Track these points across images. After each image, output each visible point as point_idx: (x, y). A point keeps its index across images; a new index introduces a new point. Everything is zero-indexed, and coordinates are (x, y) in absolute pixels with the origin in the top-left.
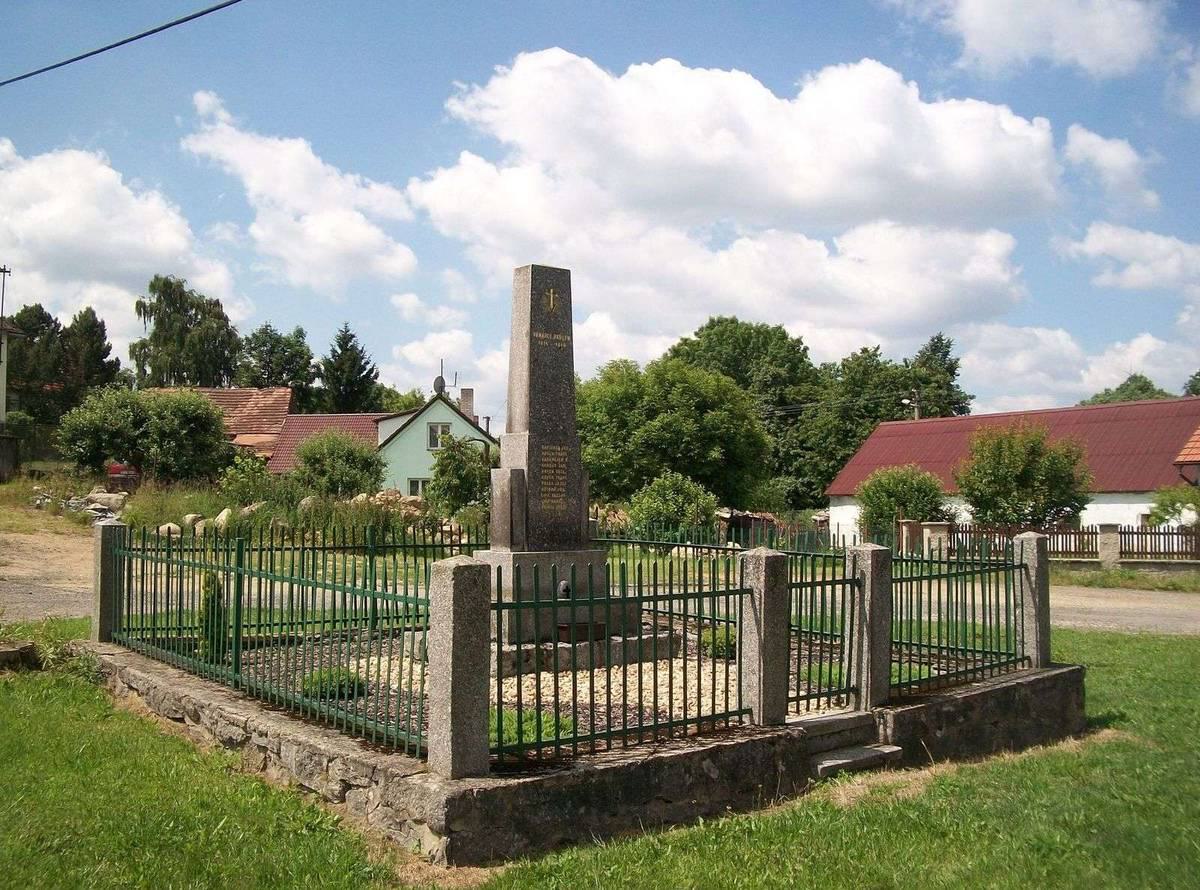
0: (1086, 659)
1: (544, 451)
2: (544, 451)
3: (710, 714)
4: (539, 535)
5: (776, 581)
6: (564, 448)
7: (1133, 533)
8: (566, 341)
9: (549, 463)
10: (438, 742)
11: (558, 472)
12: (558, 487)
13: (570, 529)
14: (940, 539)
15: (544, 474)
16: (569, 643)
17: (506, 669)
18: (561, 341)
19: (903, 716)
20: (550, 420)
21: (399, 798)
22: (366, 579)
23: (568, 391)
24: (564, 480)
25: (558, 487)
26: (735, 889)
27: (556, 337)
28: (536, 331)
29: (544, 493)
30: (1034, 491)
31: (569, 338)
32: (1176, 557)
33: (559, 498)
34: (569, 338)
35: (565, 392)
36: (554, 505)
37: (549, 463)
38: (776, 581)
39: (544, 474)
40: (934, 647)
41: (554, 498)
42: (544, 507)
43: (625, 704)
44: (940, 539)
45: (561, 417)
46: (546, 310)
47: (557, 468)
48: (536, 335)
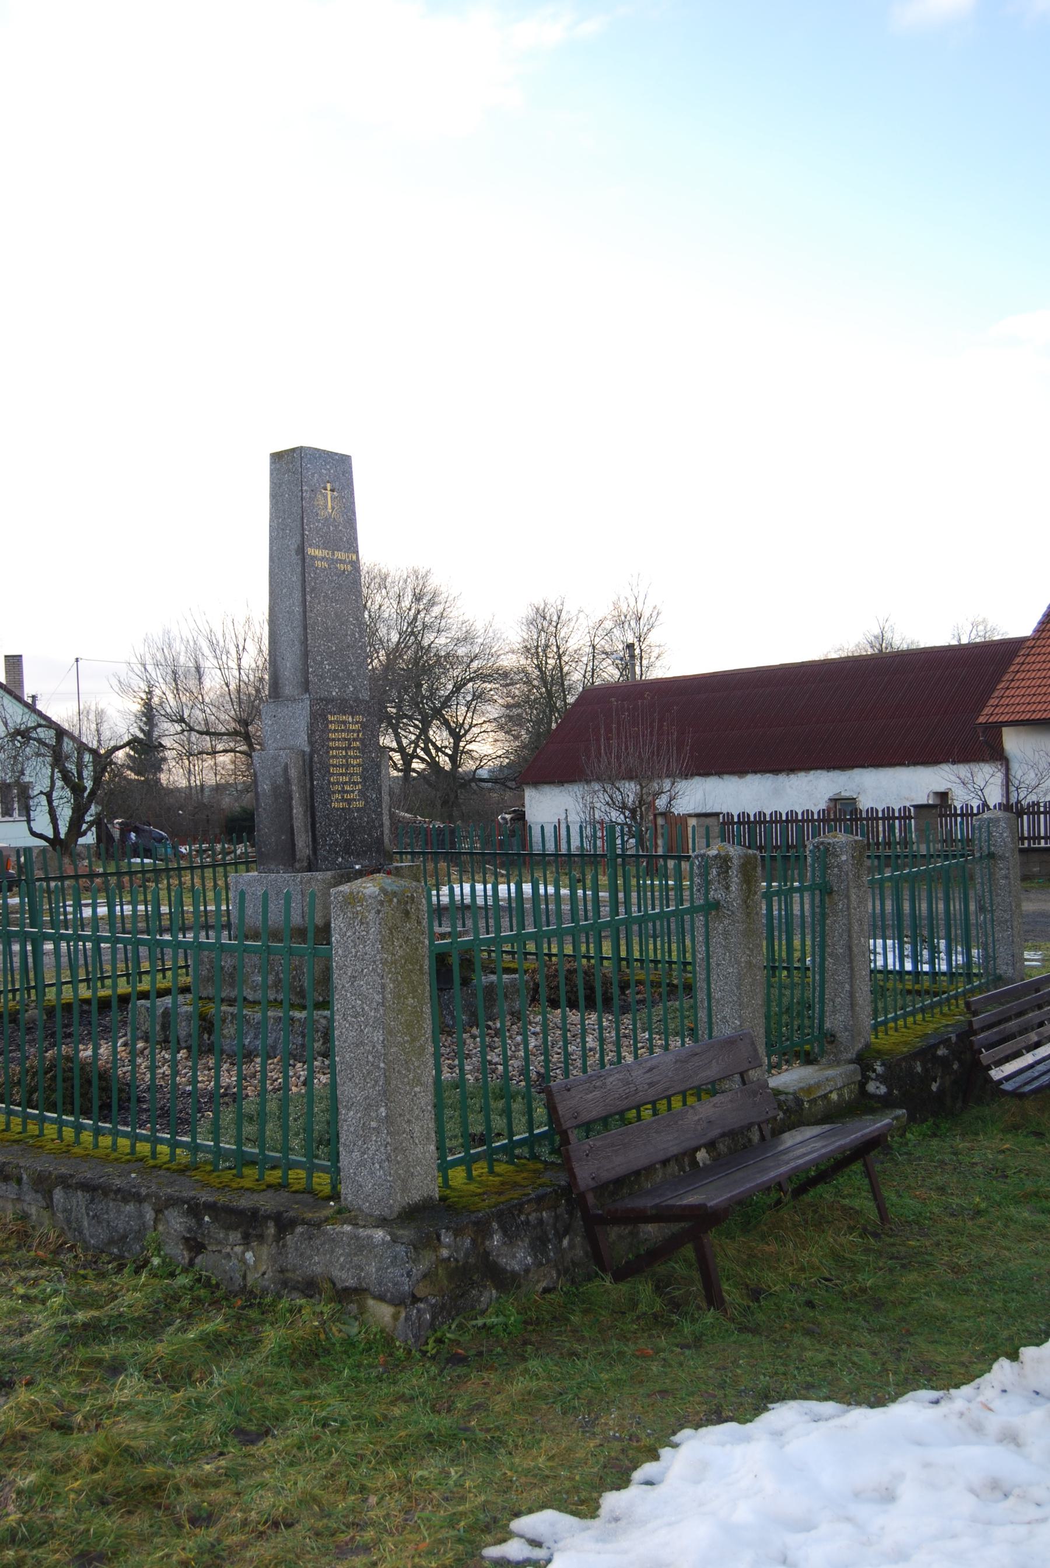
0: (425, 951)
2: (331, 722)
4: (331, 845)
5: (750, 891)
6: (358, 718)
7: (877, 819)
9: (339, 740)
10: (362, 1164)
11: (351, 753)
13: (370, 835)
14: (707, 828)
15: (334, 757)
20: (335, 677)
21: (310, 1257)
22: (684, 936)
23: (357, 635)
24: (359, 765)
25: (352, 775)
26: (1, 1267)
27: (339, 555)
30: (115, 776)
31: (354, 558)
32: (1043, 841)
33: (353, 792)
34: (354, 558)
37: (339, 740)
38: (750, 891)
39: (334, 757)
40: (607, 958)
41: (347, 792)
42: (335, 805)
44: (707, 828)
45: (350, 673)
46: (322, 513)
47: (348, 748)
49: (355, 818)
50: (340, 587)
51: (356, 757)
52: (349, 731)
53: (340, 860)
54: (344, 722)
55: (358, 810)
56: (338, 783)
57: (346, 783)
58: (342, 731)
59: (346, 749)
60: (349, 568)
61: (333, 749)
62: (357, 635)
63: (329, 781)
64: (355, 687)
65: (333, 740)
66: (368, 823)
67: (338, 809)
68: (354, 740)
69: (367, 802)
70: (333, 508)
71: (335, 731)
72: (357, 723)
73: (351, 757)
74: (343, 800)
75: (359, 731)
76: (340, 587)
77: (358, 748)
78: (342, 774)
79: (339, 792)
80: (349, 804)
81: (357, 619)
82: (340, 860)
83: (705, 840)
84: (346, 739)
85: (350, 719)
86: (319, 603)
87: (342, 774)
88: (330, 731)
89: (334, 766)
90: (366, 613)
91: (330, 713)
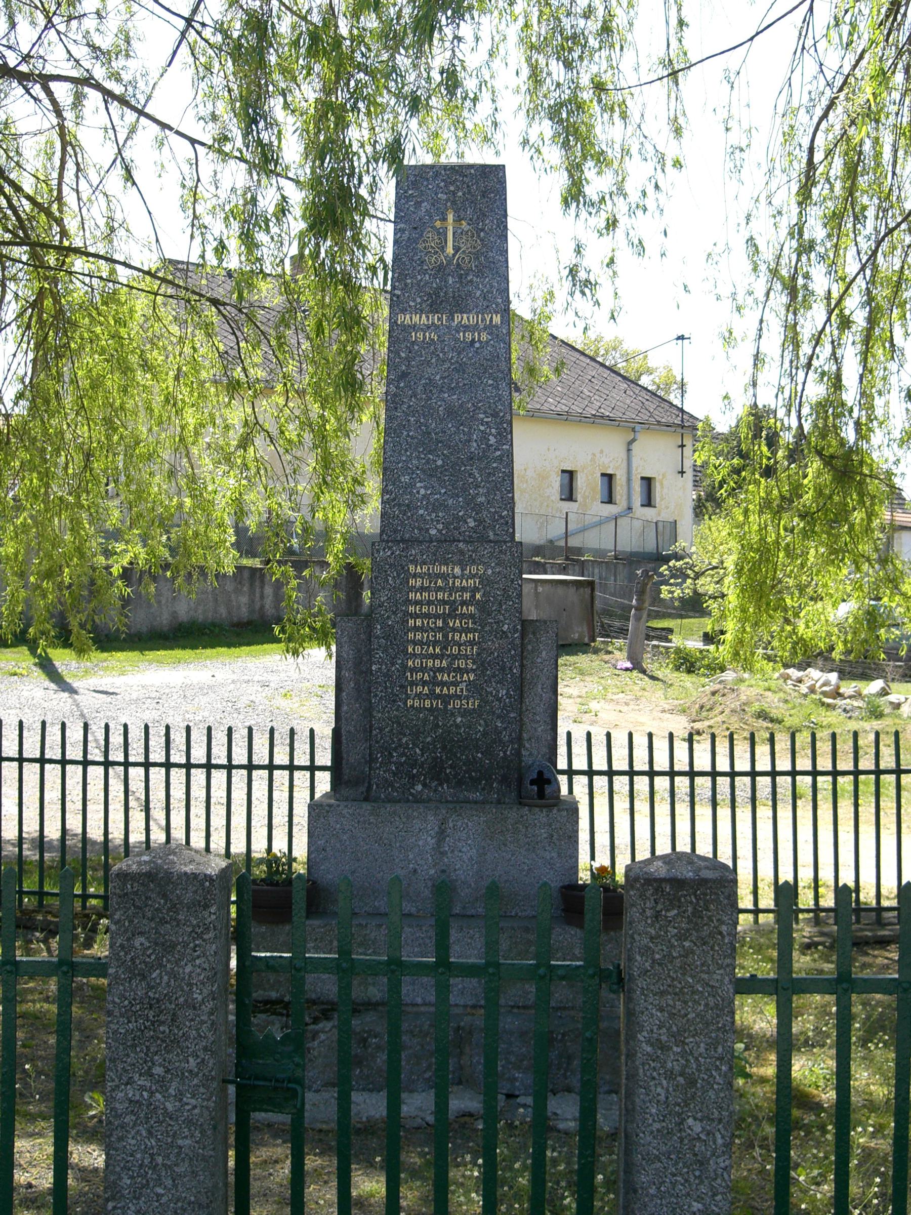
1: (415, 576)
2: (415, 576)
3: (4, 755)
4: (399, 765)
8: (490, 328)
12: (455, 657)
15: (416, 629)
16: (256, 957)
17: (259, 372)
18: (474, 328)
19: (272, 962)
25: (455, 657)
28: (404, 311)
29: (413, 670)
35: (484, 437)
36: (446, 699)
37: (429, 603)
41: (443, 684)
43: (489, 1153)
47: (452, 615)
48: (405, 319)
49: (458, 726)
50: (461, 368)
51: (467, 631)
52: (453, 589)
53: (419, 787)
54: (444, 577)
55: (465, 713)
56: (423, 669)
57: (441, 670)
58: (439, 589)
59: (445, 617)
60: (484, 337)
61: (416, 616)
62: (492, 440)
63: (404, 667)
64: (480, 522)
65: (417, 603)
66: (485, 734)
67: (419, 710)
68: (464, 603)
69: (484, 701)
70: (457, 249)
71: (422, 589)
72: (472, 576)
73: (454, 630)
74: (432, 695)
75: (475, 590)
76: (461, 368)
77: (472, 616)
78: (434, 657)
79: (424, 683)
80: (446, 703)
81: (495, 415)
82: (419, 787)
83: (143, 814)
84: (444, 602)
85: (457, 570)
86: (415, 395)
87: (434, 657)
88: (412, 589)
89: (415, 643)
90: (868, 278)
91: (415, 562)
